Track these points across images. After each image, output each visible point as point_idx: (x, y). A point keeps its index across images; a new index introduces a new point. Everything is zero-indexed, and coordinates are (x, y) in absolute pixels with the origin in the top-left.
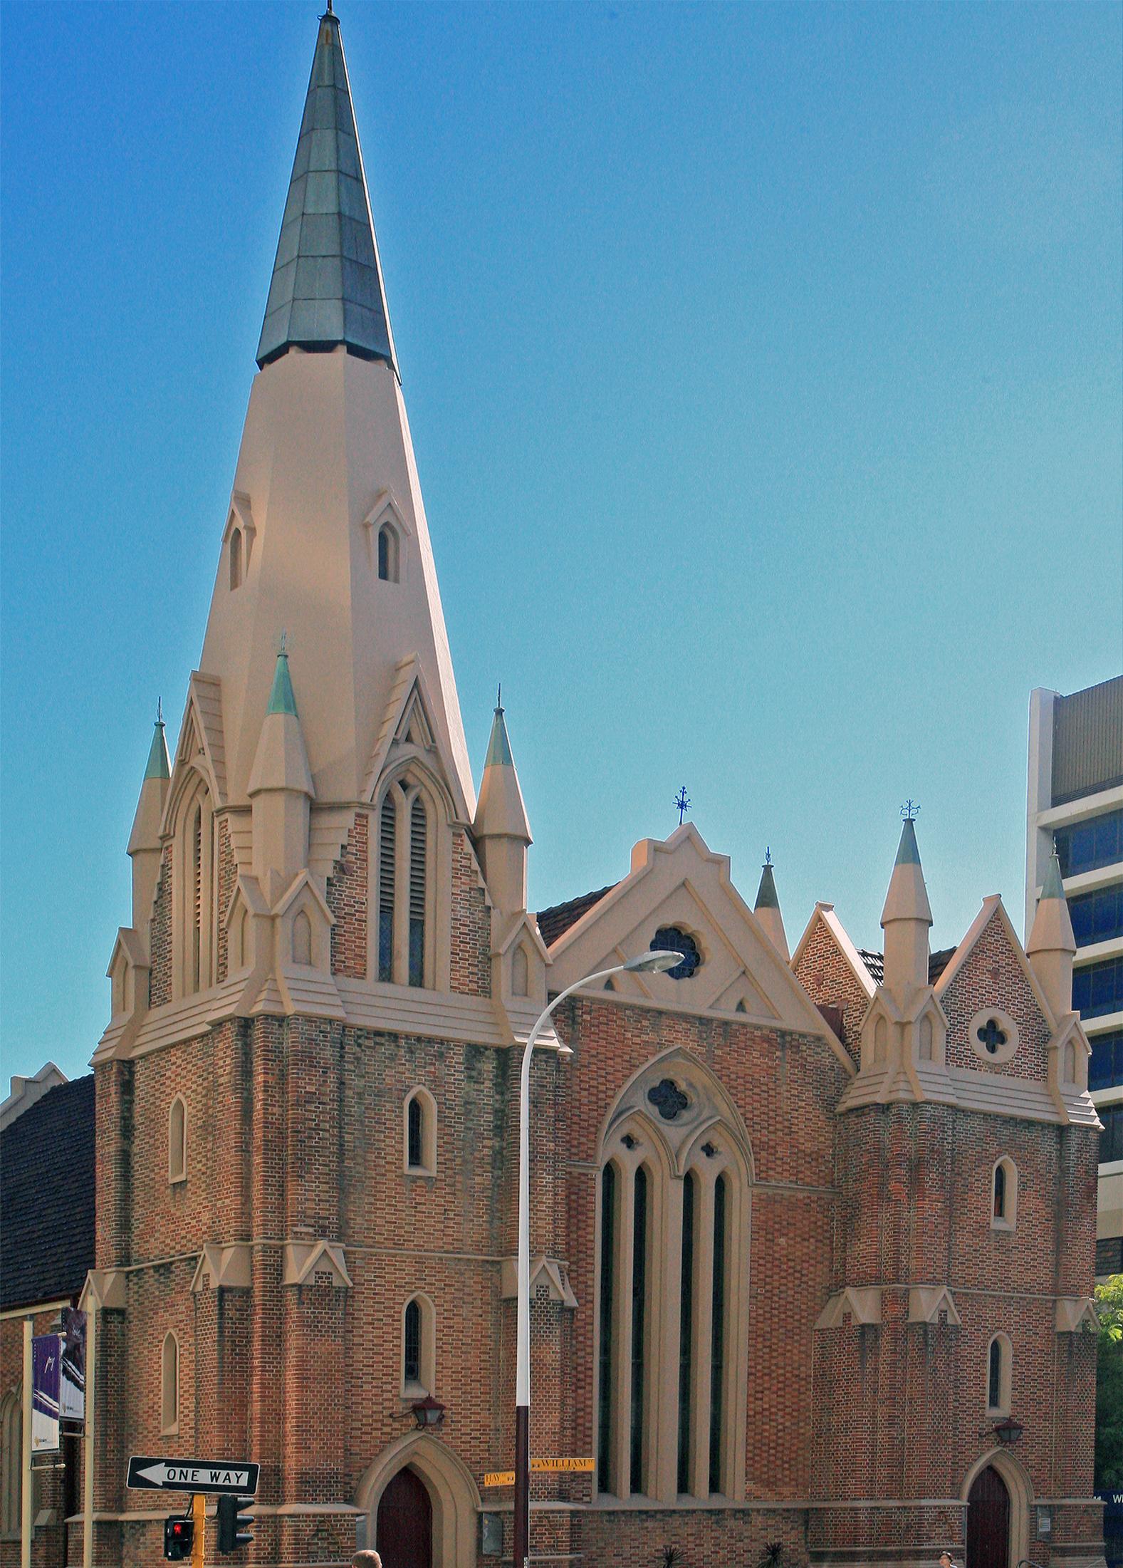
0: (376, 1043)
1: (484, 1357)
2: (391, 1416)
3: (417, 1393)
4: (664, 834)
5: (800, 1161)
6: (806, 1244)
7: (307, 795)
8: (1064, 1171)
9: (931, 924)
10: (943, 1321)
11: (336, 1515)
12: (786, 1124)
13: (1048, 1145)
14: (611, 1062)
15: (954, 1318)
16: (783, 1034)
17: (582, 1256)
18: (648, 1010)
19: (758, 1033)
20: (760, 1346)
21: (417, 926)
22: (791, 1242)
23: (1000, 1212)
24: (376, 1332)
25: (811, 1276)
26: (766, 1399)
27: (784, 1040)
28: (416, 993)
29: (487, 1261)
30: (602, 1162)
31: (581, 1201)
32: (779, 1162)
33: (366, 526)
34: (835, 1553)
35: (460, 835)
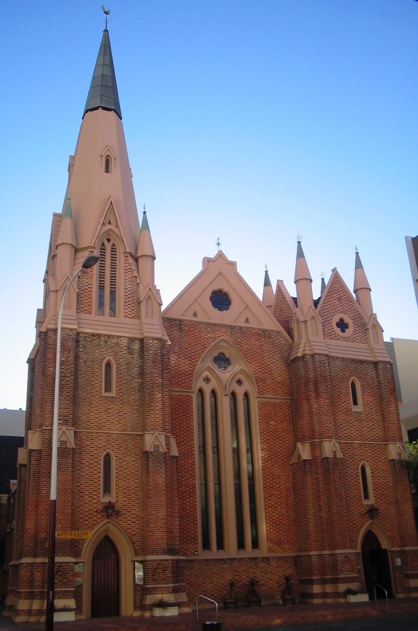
0: (92, 340)
1: (137, 481)
2: (96, 511)
3: (106, 499)
4: (212, 255)
5: (277, 386)
6: (282, 424)
7: (72, 245)
8: (379, 382)
9: (312, 282)
10: (335, 456)
11: (65, 563)
12: (269, 369)
13: (371, 372)
14: (196, 346)
15: (340, 455)
16: (264, 331)
17: (189, 433)
18: (210, 324)
19: (254, 331)
20: (267, 474)
21: (113, 293)
22: (276, 423)
23: (355, 403)
24: (91, 470)
25: (286, 439)
26: (272, 500)
27: (264, 334)
28: (112, 319)
29: (137, 435)
30: (197, 389)
31: (187, 408)
32: (268, 387)
33: (102, 156)
34: (331, 579)
35: (128, 257)
